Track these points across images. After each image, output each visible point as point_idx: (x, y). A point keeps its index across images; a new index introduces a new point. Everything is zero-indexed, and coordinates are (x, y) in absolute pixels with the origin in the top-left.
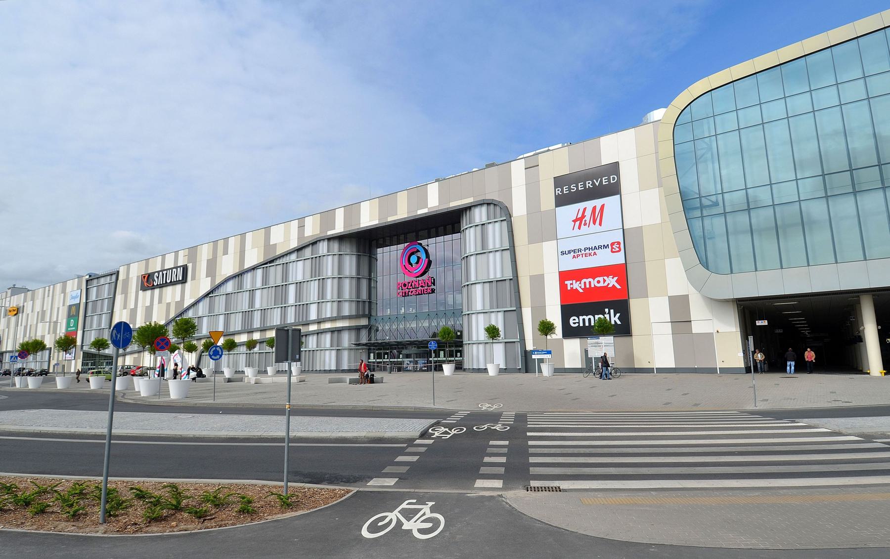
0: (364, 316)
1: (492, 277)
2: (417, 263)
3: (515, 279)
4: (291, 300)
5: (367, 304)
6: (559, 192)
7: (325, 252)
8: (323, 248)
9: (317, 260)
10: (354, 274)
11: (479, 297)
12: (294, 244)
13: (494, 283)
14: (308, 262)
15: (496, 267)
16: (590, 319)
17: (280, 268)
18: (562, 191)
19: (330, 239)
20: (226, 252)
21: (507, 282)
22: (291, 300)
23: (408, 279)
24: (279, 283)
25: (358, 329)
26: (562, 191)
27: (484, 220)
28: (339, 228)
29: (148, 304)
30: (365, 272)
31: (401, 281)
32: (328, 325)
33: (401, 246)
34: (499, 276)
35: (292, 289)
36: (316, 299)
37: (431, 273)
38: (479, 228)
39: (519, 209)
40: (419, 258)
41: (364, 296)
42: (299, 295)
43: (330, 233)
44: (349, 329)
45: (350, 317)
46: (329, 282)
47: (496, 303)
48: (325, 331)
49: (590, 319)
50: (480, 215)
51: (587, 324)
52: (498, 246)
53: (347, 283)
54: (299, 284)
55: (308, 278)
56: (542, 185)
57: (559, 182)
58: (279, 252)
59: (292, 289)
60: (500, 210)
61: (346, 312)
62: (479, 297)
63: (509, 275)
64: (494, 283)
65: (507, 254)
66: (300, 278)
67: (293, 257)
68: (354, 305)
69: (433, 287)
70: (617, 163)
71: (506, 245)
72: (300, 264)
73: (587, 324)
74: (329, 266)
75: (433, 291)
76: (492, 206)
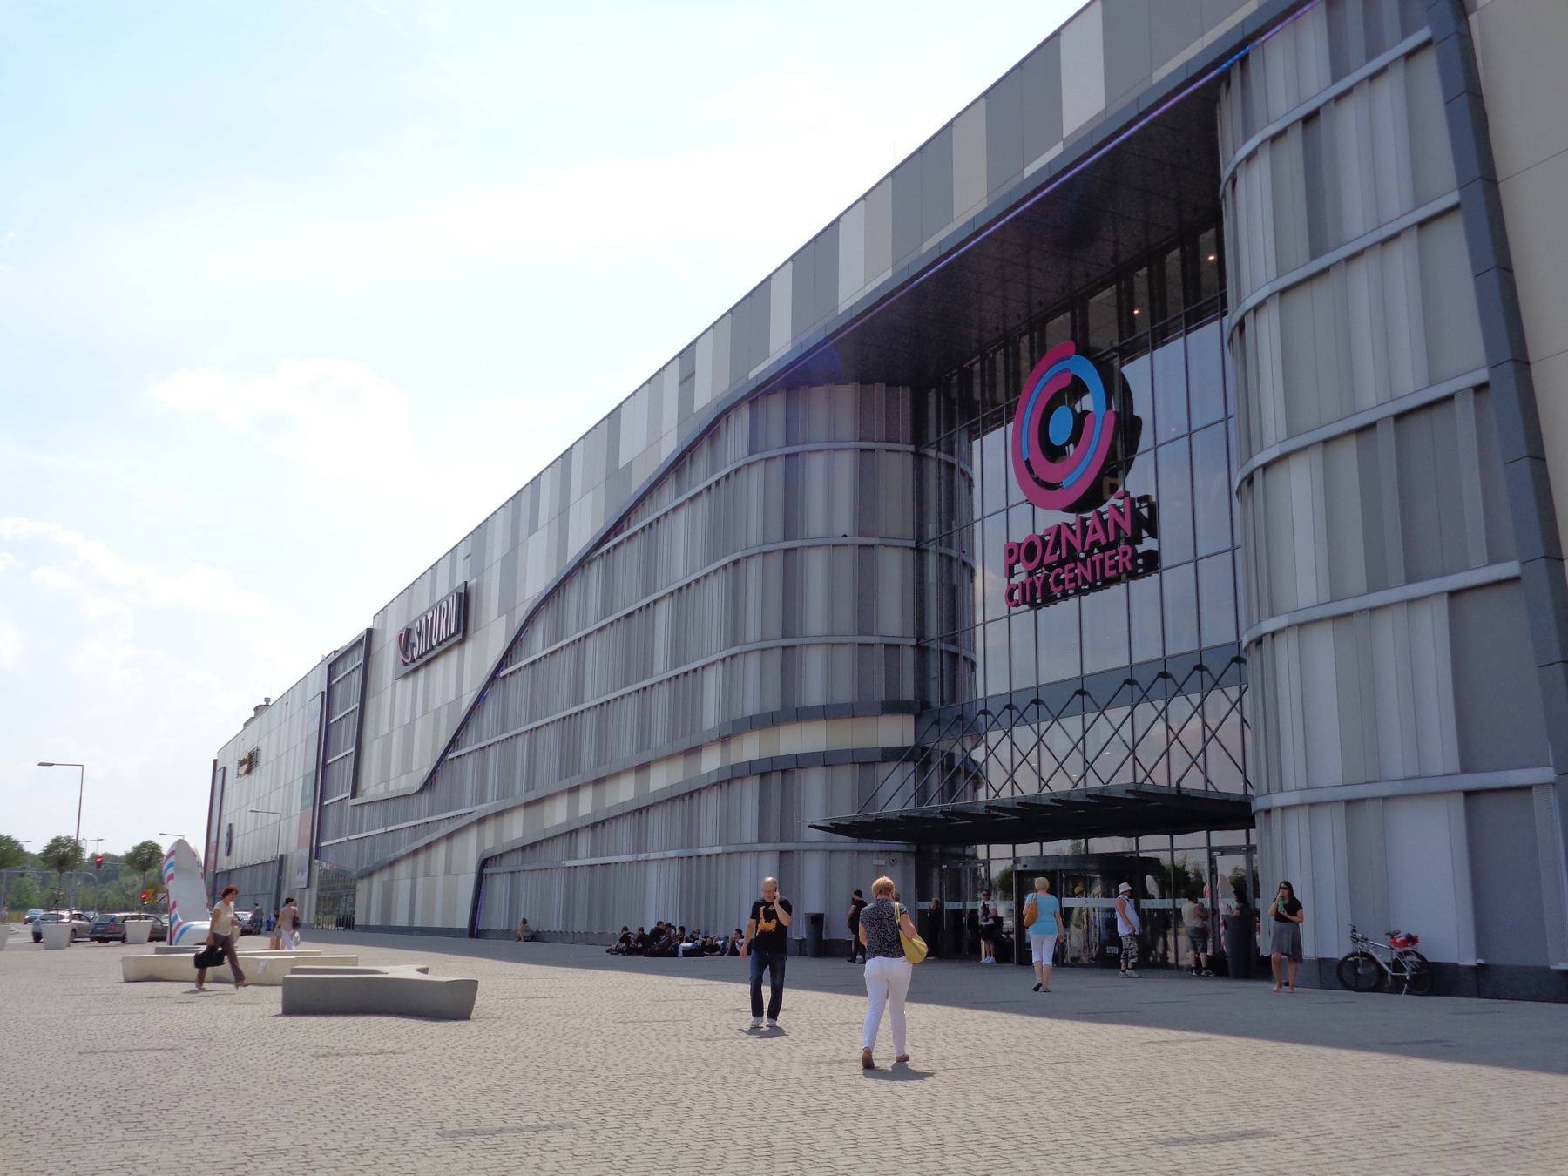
0: (892, 707)
1: (1373, 402)
2: (1075, 438)
5: (908, 659)
10: (844, 522)
20: (534, 528)
21: (1464, 410)
23: (1051, 518)
25: (865, 761)
27: (1316, 86)
29: (407, 720)
30: (896, 515)
31: (1020, 535)
33: (841, 309)
34: (1412, 388)
36: (1442, 752)
37: (1137, 481)
38: (1293, 146)
40: (1080, 418)
41: (894, 621)
44: (827, 760)
45: (826, 712)
53: (815, 565)
61: (814, 694)
63: (1468, 361)
64: (1386, 437)
65: (1453, 241)
67: (667, 499)
68: (845, 658)
69: (1148, 544)
75: (1151, 562)
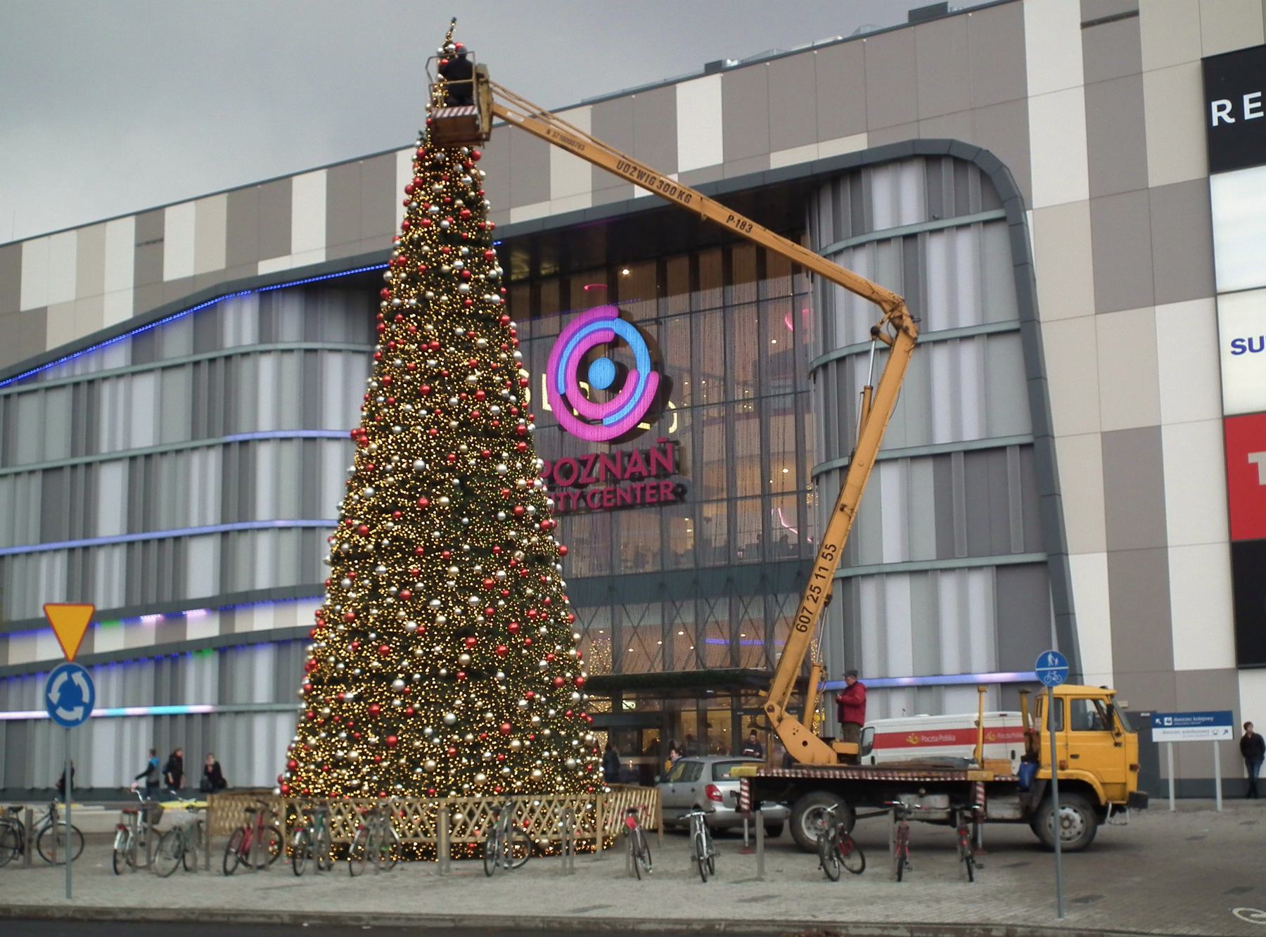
1: (943, 437)
3: (1037, 449)
4: (111, 518)
6: (1222, 112)
7: (248, 337)
8: (240, 324)
9: (216, 375)
11: (893, 513)
12: (119, 308)
13: (957, 463)
14: (180, 382)
15: (960, 399)
16: (1252, 101)
17: (60, 404)
18: (1237, 111)
19: (269, 290)
21: (1013, 458)
22: (111, 518)
24: (58, 453)
26: (1237, 111)
27: (911, 215)
28: (308, 246)
32: (263, 620)
34: (971, 433)
35: (112, 486)
39: (1057, 173)
42: (140, 504)
43: (266, 267)
46: (265, 455)
47: (956, 543)
48: (252, 641)
49: (1252, 101)
50: (896, 200)
51: (1258, 104)
52: (967, 319)
54: (141, 464)
55: (178, 434)
56: (1152, 85)
57: (1223, 75)
58: (56, 338)
59: (112, 486)
60: (980, 181)
62: (893, 513)
65: (1007, 353)
66: (143, 439)
67: (117, 357)
69: (674, 480)
70: (1105, 435)
71: (1003, 313)
72: (145, 387)
73: (1258, 104)
74: (267, 394)
76: (947, 170)
